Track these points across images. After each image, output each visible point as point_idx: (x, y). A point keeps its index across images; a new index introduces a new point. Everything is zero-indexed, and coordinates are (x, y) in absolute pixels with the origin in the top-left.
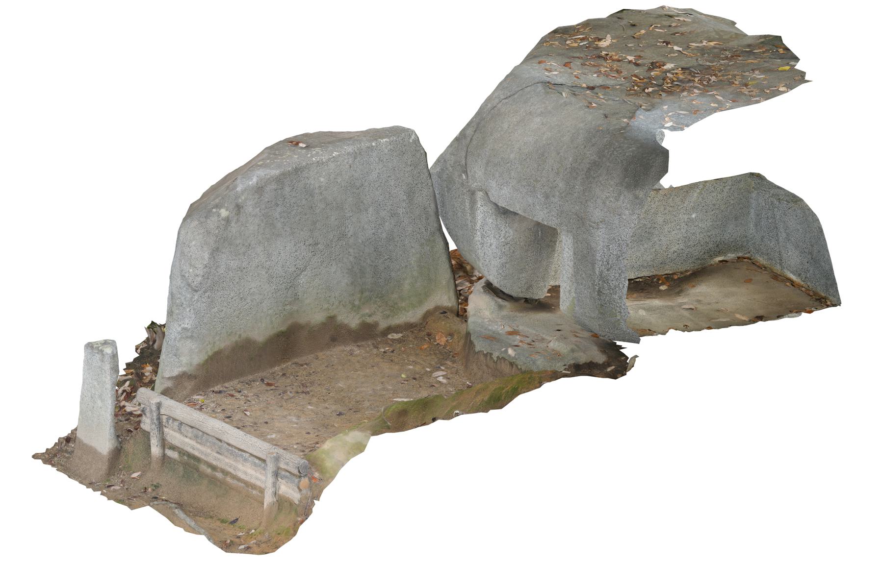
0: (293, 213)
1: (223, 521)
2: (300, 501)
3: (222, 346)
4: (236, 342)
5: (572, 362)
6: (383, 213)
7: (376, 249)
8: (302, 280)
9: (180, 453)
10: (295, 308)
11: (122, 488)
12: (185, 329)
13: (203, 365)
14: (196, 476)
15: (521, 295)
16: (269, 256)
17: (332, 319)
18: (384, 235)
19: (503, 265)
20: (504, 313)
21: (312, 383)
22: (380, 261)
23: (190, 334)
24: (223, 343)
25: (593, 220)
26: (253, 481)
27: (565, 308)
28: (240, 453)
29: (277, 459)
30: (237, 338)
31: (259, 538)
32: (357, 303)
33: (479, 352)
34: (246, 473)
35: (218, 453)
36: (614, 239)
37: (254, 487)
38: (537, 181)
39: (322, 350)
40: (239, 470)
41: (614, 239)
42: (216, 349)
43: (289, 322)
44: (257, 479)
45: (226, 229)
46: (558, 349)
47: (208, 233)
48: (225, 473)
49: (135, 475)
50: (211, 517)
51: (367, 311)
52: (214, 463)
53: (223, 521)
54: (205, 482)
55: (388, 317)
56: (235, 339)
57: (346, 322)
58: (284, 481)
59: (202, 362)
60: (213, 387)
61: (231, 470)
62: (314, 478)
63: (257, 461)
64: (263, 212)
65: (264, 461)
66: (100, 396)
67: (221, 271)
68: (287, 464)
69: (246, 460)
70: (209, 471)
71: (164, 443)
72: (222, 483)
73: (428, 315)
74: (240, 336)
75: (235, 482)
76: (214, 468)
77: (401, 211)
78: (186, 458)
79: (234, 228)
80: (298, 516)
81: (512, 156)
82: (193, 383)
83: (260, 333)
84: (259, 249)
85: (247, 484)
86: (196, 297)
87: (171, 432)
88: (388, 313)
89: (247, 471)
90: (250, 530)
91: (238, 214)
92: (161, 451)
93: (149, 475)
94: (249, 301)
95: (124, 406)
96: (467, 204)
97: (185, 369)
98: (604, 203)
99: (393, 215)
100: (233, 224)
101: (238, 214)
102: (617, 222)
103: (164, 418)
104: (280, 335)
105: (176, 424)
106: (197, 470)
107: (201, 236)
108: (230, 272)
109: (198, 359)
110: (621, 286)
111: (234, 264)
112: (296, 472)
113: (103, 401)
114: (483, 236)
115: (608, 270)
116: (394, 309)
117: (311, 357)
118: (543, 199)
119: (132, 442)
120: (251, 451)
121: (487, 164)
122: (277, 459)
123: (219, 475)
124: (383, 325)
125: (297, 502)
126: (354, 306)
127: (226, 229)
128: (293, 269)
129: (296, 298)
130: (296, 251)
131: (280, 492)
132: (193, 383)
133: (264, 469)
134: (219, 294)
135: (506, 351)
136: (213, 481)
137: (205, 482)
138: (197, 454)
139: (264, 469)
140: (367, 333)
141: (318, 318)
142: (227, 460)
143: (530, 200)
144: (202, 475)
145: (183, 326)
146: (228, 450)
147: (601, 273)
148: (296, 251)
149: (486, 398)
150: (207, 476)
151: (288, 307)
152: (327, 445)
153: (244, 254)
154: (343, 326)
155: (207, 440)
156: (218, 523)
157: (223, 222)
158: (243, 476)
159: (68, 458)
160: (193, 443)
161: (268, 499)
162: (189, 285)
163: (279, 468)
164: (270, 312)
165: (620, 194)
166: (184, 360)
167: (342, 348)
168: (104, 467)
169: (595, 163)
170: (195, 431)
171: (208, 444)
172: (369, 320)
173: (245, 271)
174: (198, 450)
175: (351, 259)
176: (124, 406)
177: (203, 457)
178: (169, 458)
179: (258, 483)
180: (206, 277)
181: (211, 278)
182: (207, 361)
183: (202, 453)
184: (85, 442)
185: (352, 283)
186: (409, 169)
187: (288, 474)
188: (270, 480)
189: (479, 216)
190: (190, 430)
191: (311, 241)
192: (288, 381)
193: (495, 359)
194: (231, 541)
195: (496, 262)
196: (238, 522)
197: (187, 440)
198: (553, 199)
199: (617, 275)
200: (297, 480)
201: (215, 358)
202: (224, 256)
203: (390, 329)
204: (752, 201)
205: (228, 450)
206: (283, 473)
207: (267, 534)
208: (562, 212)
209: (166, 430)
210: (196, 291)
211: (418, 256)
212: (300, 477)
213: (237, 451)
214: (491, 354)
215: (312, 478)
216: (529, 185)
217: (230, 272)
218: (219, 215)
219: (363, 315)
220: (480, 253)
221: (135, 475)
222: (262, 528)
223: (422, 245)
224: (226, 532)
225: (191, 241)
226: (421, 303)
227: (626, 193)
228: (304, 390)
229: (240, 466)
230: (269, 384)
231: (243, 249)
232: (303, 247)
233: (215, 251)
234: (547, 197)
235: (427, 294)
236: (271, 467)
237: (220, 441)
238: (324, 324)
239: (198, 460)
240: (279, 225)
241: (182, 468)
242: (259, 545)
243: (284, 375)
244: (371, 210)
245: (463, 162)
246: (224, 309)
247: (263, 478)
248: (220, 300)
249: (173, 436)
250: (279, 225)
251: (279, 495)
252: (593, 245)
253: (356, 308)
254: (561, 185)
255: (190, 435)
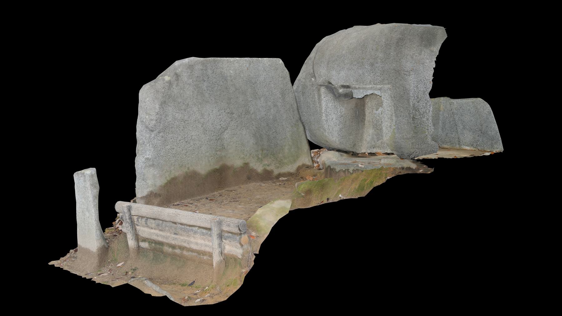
0: (216, 88)
1: (183, 285)
2: (243, 255)
3: (177, 174)
4: (186, 172)
5: (401, 166)
6: (269, 103)
7: (268, 125)
8: (226, 135)
9: (149, 242)
10: (223, 154)
11: (109, 274)
12: (147, 159)
13: (164, 186)
14: (162, 257)
15: (351, 150)
16: (202, 115)
17: (246, 164)
18: (271, 117)
19: (341, 130)
20: (344, 158)
21: (239, 197)
22: (271, 133)
23: (151, 163)
24: (178, 172)
25: (406, 69)
26: (203, 249)
27: (388, 138)
28: (191, 228)
29: (220, 223)
30: (186, 169)
31: (212, 291)
32: (260, 156)
33: (339, 171)
34: (197, 244)
35: (175, 234)
36: (421, 80)
37: (204, 253)
38: (363, 59)
39: (243, 184)
40: (192, 242)
41: (421, 80)
42: (172, 176)
43: (221, 163)
44: (206, 246)
45: (169, 89)
46: (388, 162)
47: (157, 91)
48: (182, 248)
49: (120, 265)
50: (174, 284)
51: (266, 162)
52: (173, 242)
53: (183, 285)
54: (169, 259)
55: (278, 167)
56: (186, 170)
57: (255, 168)
58: (227, 242)
59: (163, 184)
60: (174, 202)
61: (185, 245)
62: (252, 236)
63: (204, 231)
64: (195, 83)
65: (210, 229)
66: (87, 209)
67: (170, 119)
68: (229, 226)
69: (195, 233)
70: (170, 250)
71: (137, 238)
72: (181, 257)
73: (299, 168)
74: (188, 168)
75: (190, 253)
76: (173, 247)
77: (279, 104)
78: (153, 245)
79: (175, 90)
80: (242, 268)
81: (344, 52)
82: (158, 200)
83: (203, 167)
84: (195, 109)
85: (199, 252)
86: (153, 135)
87: (142, 228)
88: (278, 165)
89: (198, 242)
90: (204, 288)
91: (177, 80)
92: (136, 243)
93: (129, 262)
94: (192, 144)
95: (118, 227)
96: (316, 96)
97: (151, 189)
98: (412, 58)
99: (275, 106)
100: (174, 86)
101: (177, 80)
102: (421, 68)
103: (135, 218)
104: (215, 171)
105: (144, 220)
106: (162, 252)
107: (152, 94)
108: (176, 121)
109: (161, 182)
110: (427, 111)
111: (178, 116)
112: (236, 230)
113: (89, 211)
114: (327, 116)
115: (418, 102)
116: (281, 164)
117: (236, 188)
118: (369, 68)
119: (116, 241)
120: (198, 224)
121: (328, 64)
122: (220, 223)
123: (178, 251)
124: (276, 172)
125: (240, 257)
126: (259, 158)
127: (169, 89)
128: (219, 127)
129: (223, 148)
130: (220, 115)
131: (226, 252)
132: (158, 200)
133: (211, 236)
134: (170, 136)
135: (358, 166)
136: (174, 257)
137: (169, 259)
138: (160, 239)
139: (211, 236)
140: (267, 176)
141: (238, 163)
142: (182, 238)
143: (361, 72)
144: (166, 255)
145: (145, 157)
146: (181, 229)
147: (414, 105)
148: (220, 115)
149: (357, 187)
150: (170, 255)
151: (218, 153)
152: (259, 212)
153: (185, 110)
154: (252, 171)
155: (166, 226)
156: (180, 287)
157: (167, 84)
158: (194, 247)
159: (73, 261)
160: (157, 232)
161: (216, 258)
162: (147, 127)
163: (222, 231)
164: (207, 154)
165: (421, 51)
166: (150, 182)
167: (254, 183)
168: (95, 261)
169: (400, 39)
170: (157, 221)
171: (167, 228)
172: (268, 168)
173: (187, 122)
174: (161, 235)
175: (254, 127)
176: (118, 227)
177: (164, 240)
178: (143, 248)
179: (208, 249)
180: (159, 121)
181: (163, 122)
182: (167, 184)
183: (164, 237)
184: (83, 246)
185: (256, 143)
186: (280, 79)
187: (230, 234)
188: (216, 241)
189: (324, 104)
190: (153, 221)
191: (228, 111)
192: (224, 198)
193: (352, 172)
194: (189, 297)
195: (337, 128)
196: (195, 284)
197: (153, 231)
198: (377, 65)
199: (424, 104)
200: (238, 238)
201: (172, 182)
202: (170, 108)
203: (280, 175)
204: (440, 116)
205: (181, 229)
206: (226, 234)
207: (218, 288)
208: (384, 71)
209: (138, 227)
210: (152, 131)
211: (291, 133)
212: (241, 234)
213: (188, 228)
214: (348, 170)
215: (250, 236)
216: (358, 63)
217: (176, 121)
218: (164, 80)
219: (264, 165)
220: (326, 126)
221: (120, 265)
222: (213, 284)
223: (292, 126)
224: (185, 292)
225: (146, 99)
226: (295, 161)
227: (425, 50)
228: (235, 200)
229: (192, 240)
230: (211, 200)
231: (184, 107)
232: (224, 114)
233: (163, 104)
234: (372, 65)
235: (296, 158)
236: (215, 231)
237: (175, 223)
238: (242, 167)
239: (161, 244)
240: (207, 95)
241: (152, 254)
242: (212, 297)
243: (220, 195)
244: (262, 99)
245: (312, 71)
246: (175, 148)
247: (211, 244)
248: (171, 140)
249: (144, 231)
250: (207, 95)
251: (225, 255)
252: (408, 87)
253: (260, 160)
254: (381, 55)
255: (153, 226)
